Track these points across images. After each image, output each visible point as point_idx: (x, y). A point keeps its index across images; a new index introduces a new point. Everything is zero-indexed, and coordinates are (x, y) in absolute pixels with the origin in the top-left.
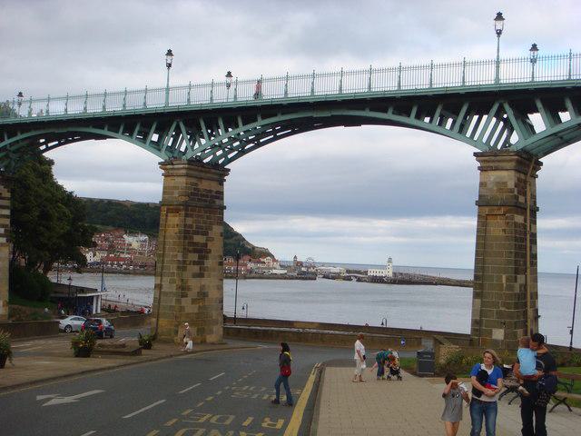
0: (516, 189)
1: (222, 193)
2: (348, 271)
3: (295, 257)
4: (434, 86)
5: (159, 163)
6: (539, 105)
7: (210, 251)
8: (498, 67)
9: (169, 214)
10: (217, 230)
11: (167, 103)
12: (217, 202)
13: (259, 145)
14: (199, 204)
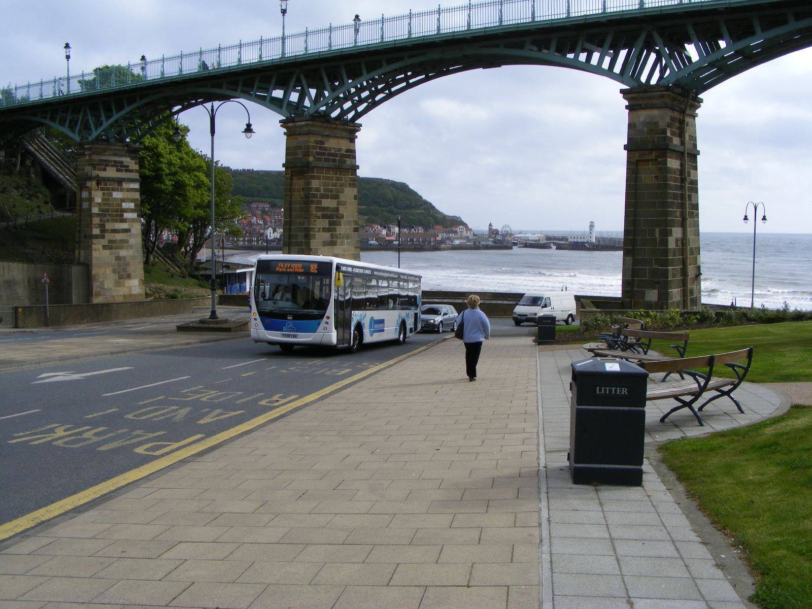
0: (669, 134)
1: (354, 151)
2: (548, 238)
3: (490, 225)
4: (608, 11)
5: (280, 122)
6: (691, 31)
7: (342, 217)
8: (283, 43)
9: (294, 178)
10: (349, 193)
11: (283, 53)
12: (348, 161)
13: (391, 95)
14: (326, 164)
